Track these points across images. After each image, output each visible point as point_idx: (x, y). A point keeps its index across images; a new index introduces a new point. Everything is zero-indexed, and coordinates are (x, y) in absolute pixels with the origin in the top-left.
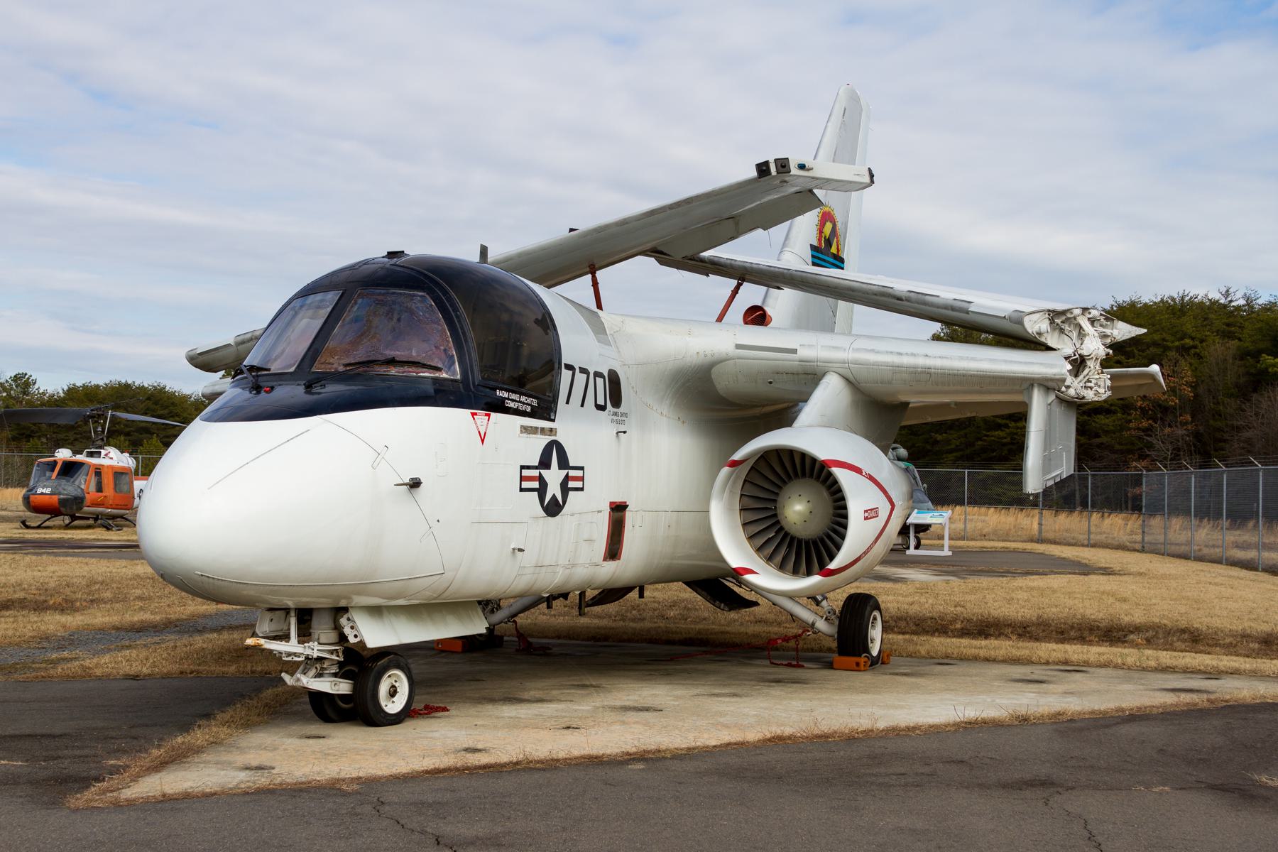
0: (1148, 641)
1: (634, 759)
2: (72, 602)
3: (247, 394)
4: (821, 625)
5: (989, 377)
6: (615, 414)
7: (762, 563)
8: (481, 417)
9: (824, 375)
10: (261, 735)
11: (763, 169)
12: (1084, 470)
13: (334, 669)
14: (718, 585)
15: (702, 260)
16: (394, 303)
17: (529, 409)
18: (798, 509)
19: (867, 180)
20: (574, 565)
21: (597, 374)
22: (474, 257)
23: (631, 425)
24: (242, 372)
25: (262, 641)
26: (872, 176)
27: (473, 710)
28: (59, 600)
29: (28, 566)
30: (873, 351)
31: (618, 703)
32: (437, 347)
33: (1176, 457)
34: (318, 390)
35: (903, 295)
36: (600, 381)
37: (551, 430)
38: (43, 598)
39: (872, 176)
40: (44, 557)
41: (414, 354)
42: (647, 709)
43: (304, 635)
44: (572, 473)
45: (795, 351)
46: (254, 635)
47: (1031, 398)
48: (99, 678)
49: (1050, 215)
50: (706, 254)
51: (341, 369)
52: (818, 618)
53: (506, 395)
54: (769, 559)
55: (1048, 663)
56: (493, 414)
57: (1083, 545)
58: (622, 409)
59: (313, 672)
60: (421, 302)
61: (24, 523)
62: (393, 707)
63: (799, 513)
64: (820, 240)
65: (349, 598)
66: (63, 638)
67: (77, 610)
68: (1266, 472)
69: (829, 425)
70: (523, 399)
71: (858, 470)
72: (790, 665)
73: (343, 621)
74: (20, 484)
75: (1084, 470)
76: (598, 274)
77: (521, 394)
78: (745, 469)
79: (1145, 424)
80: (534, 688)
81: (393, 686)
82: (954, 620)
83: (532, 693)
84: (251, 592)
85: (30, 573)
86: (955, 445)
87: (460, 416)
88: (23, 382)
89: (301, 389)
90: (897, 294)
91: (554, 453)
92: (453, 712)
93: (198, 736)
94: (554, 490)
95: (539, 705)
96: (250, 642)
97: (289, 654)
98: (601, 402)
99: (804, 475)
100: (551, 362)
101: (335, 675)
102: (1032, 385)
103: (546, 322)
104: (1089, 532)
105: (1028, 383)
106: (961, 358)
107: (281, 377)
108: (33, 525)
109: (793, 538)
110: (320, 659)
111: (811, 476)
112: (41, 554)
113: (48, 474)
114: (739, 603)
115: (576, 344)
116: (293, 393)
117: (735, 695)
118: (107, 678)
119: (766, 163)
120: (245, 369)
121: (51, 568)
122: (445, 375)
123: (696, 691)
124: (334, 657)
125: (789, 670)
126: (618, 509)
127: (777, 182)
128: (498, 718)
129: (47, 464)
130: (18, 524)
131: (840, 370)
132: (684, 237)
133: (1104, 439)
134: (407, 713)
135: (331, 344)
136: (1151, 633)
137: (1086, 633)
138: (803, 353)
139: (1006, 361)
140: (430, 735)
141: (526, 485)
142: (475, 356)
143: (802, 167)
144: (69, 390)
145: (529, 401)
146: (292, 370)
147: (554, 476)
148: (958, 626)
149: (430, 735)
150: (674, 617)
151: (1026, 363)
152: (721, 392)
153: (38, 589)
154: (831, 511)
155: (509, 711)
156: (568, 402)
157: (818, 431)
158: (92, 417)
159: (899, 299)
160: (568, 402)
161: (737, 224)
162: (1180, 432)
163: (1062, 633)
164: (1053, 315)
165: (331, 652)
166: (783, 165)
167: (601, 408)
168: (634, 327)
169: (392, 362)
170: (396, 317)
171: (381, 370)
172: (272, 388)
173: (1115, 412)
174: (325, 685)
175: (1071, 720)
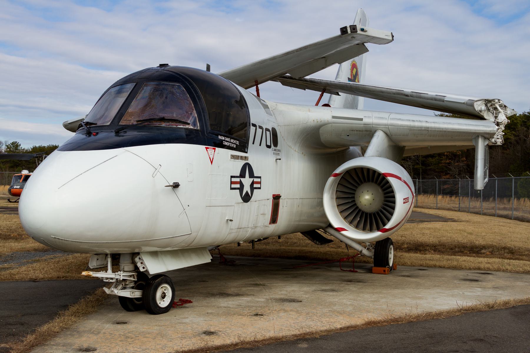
0: (492, 253)
1: (300, 340)
2: (21, 235)
3: (84, 136)
4: (365, 252)
5: (458, 132)
6: (275, 150)
7: (347, 224)
8: (211, 150)
9: (375, 131)
10: (92, 321)
11: (344, 30)
12: (493, 177)
13: (132, 285)
14: (316, 231)
15: (306, 81)
16: (164, 89)
17: (235, 146)
18: (367, 198)
19: (391, 38)
20: (256, 227)
21: (267, 130)
22: (204, 69)
23: (282, 156)
24: (82, 126)
25: (91, 273)
26: (393, 37)
27: (205, 302)
28: (16, 234)
29: (5, 219)
30: (400, 119)
31: (278, 297)
32: (187, 112)
33: (459, 174)
34: (122, 134)
35: (409, 94)
36: (268, 133)
37: (246, 157)
38: (9, 233)
39: (393, 37)
40: (12, 215)
41: (175, 115)
42: (293, 301)
43: (116, 268)
44: (256, 180)
45: (362, 119)
46: (88, 269)
47: (477, 143)
48: (17, 281)
49: (451, 67)
50: (308, 77)
51: (135, 123)
52: (364, 248)
53: (223, 138)
54: (351, 223)
55: (470, 269)
56: (217, 149)
57: (434, 209)
58: (278, 148)
59: (120, 287)
60: (178, 89)
61: (9, 200)
62: (164, 304)
63: (367, 200)
64: (351, 76)
65: (140, 248)
66: (8, 255)
67: (23, 239)
68: (515, 179)
69: (380, 156)
70: (232, 141)
71: (399, 178)
72: (351, 271)
73: (137, 259)
74: (9, 184)
75: (493, 177)
76: (259, 86)
77: (231, 138)
78: (340, 177)
79: (448, 161)
80: (233, 286)
81: (164, 293)
82: (403, 244)
83: (232, 289)
84: (85, 246)
85: (5, 222)
86: (437, 166)
87: (200, 149)
88: (15, 145)
89: (113, 134)
90: (406, 93)
91: (247, 169)
92: (194, 304)
93: (55, 325)
94: (247, 188)
95: (238, 298)
96: (84, 273)
97: (107, 278)
98: (269, 144)
99: (369, 181)
100: (245, 124)
101: (133, 288)
102: (478, 136)
103: (242, 103)
104: (437, 204)
105: (476, 135)
106: (444, 123)
107: (102, 128)
108: (13, 201)
109: (363, 212)
110: (124, 280)
111: (373, 181)
112: (11, 214)
113: (19, 180)
114: (324, 241)
115: (256, 114)
116: (111, 136)
117: (333, 290)
118: (22, 280)
119: (346, 27)
120: (83, 124)
121: (15, 220)
122: (191, 127)
123: (314, 288)
124: (132, 279)
125: (352, 274)
126: (276, 198)
127: (350, 37)
128: (218, 307)
129: (18, 176)
130: (7, 201)
131: (384, 129)
132: (294, 71)
133: (432, 167)
134: (172, 305)
135: (130, 110)
136: (490, 250)
137: (462, 250)
138: (366, 120)
139: (466, 124)
140: (185, 321)
141: (233, 186)
142: (207, 117)
143: (362, 30)
144: (33, 148)
145: (235, 142)
146: (108, 124)
147: (247, 181)
148: (406, 246)
149: (185, 321)
150: (282, 242)
151: (476, 125)
152: (322, 140)
153: (7, 229)
154: (383, 199)
155: (224, 302)
156: (253, 143)
157: (374, 158)
158: (37, 157)
159: (407, 96)
160: (253, 143)
161: (326, 61)
162: (461, 164)
163: (452, 249)
164: (488, 102)
165: (130, 276)
166: (354, 28)
167: (269, 147)
168: (282, 107)
169: (163, 119)
170: (165, 96)
171: (157, 124)
172: (97, 133)
173: (436, 157)
174: (127, 294)
175: (513, 307)
